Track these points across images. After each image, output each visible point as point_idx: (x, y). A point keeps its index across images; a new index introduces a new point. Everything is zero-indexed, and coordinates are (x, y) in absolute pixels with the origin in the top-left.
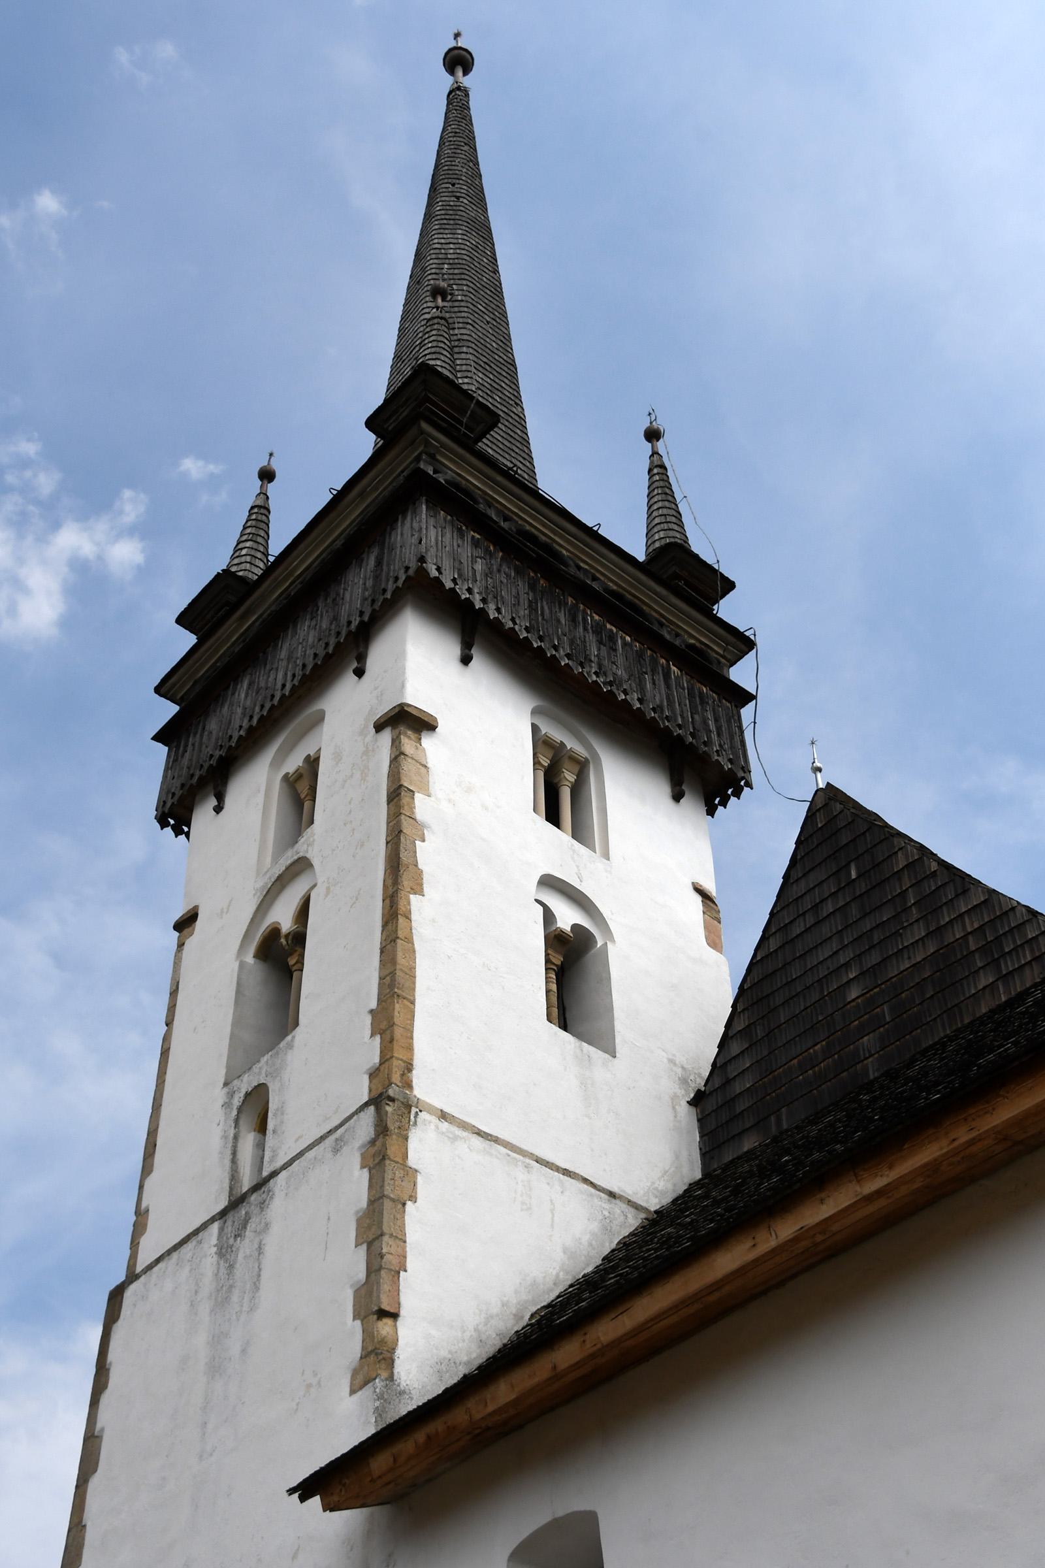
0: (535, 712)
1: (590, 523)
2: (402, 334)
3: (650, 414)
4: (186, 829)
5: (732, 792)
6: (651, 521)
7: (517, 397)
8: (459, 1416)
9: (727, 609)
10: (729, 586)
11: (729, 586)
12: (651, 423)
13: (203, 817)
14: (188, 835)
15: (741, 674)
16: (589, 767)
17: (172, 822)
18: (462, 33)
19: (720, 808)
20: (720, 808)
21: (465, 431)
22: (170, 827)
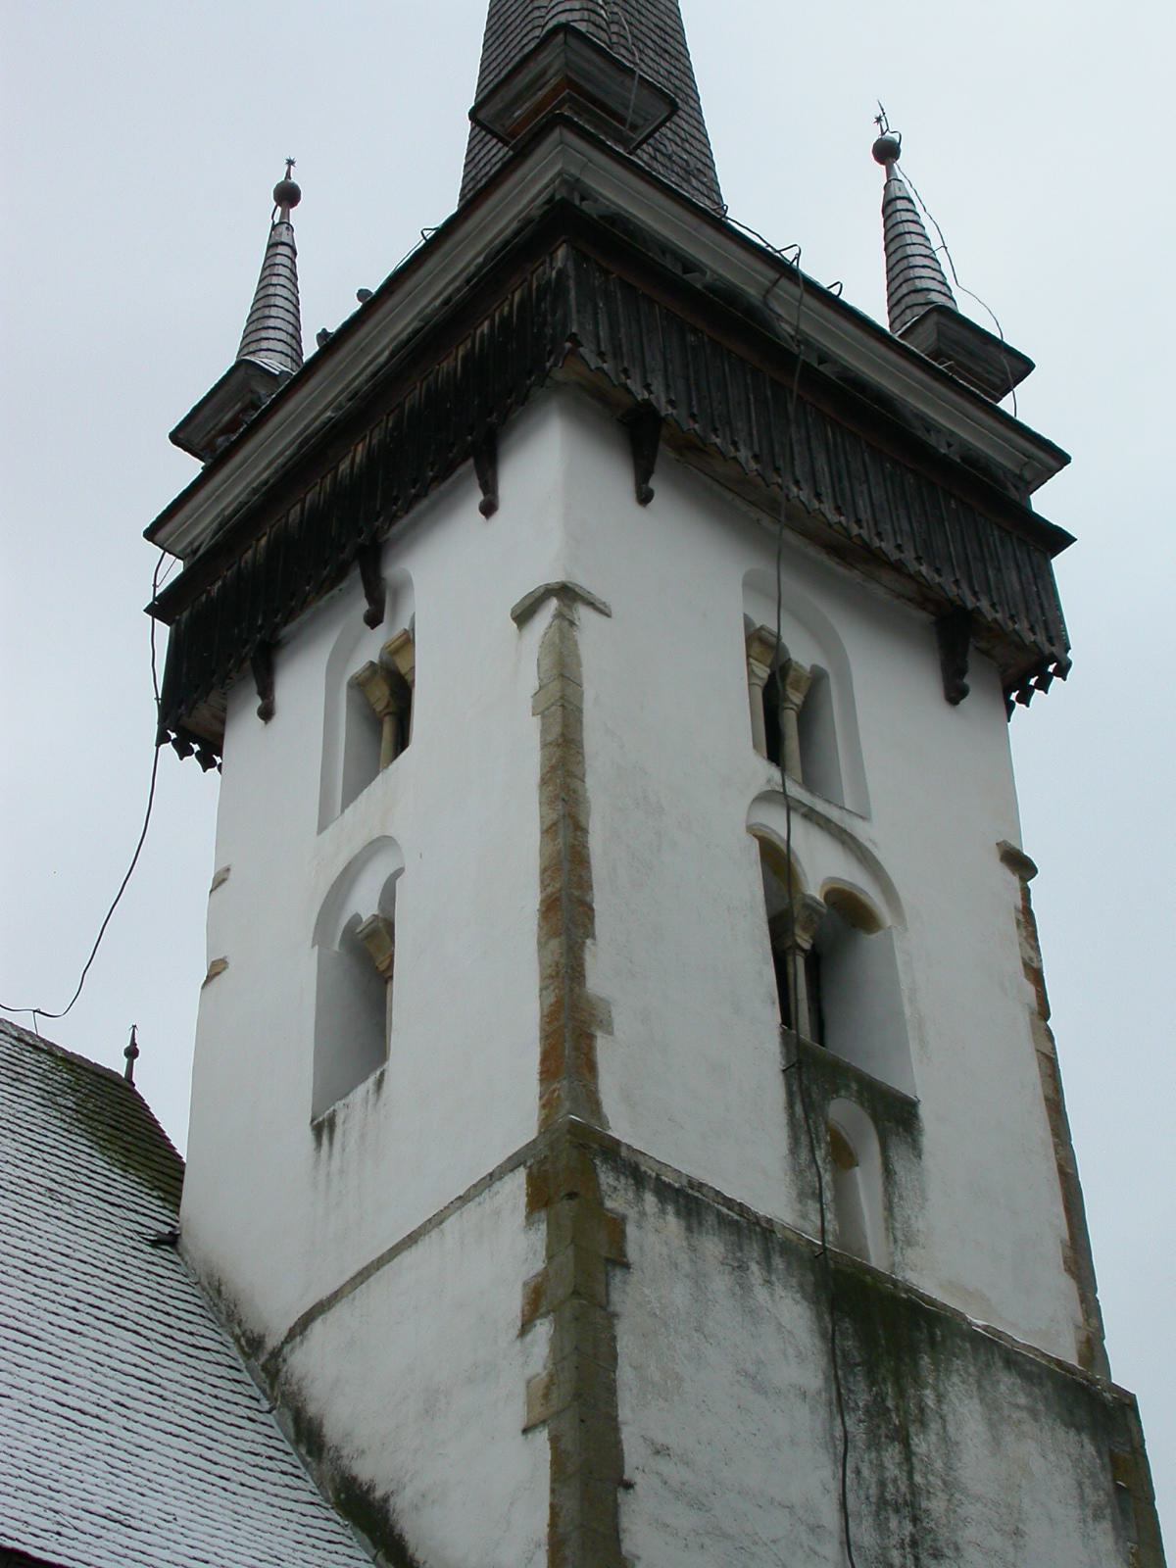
0: (750, 584)
1: (824, 283)
2: (489, 57)
3: (879, 120)
4: (218, 760)
5: (1055, 669)
6: (896, 289)
7: (684, 73)
8: (197, 421)
9: (1023, 404)
10: (1023, 366)
11: (1023, 366)
12: (883, 134)
13: (244, 733)
14: (220, 767)
15: (1047, 502)
16: (829, 692)
17: (173, 736)
18: (520, 1432)
19: (1037, 693)
20: (1037, 693)
21: (622, 128)
22: (170, 743)
